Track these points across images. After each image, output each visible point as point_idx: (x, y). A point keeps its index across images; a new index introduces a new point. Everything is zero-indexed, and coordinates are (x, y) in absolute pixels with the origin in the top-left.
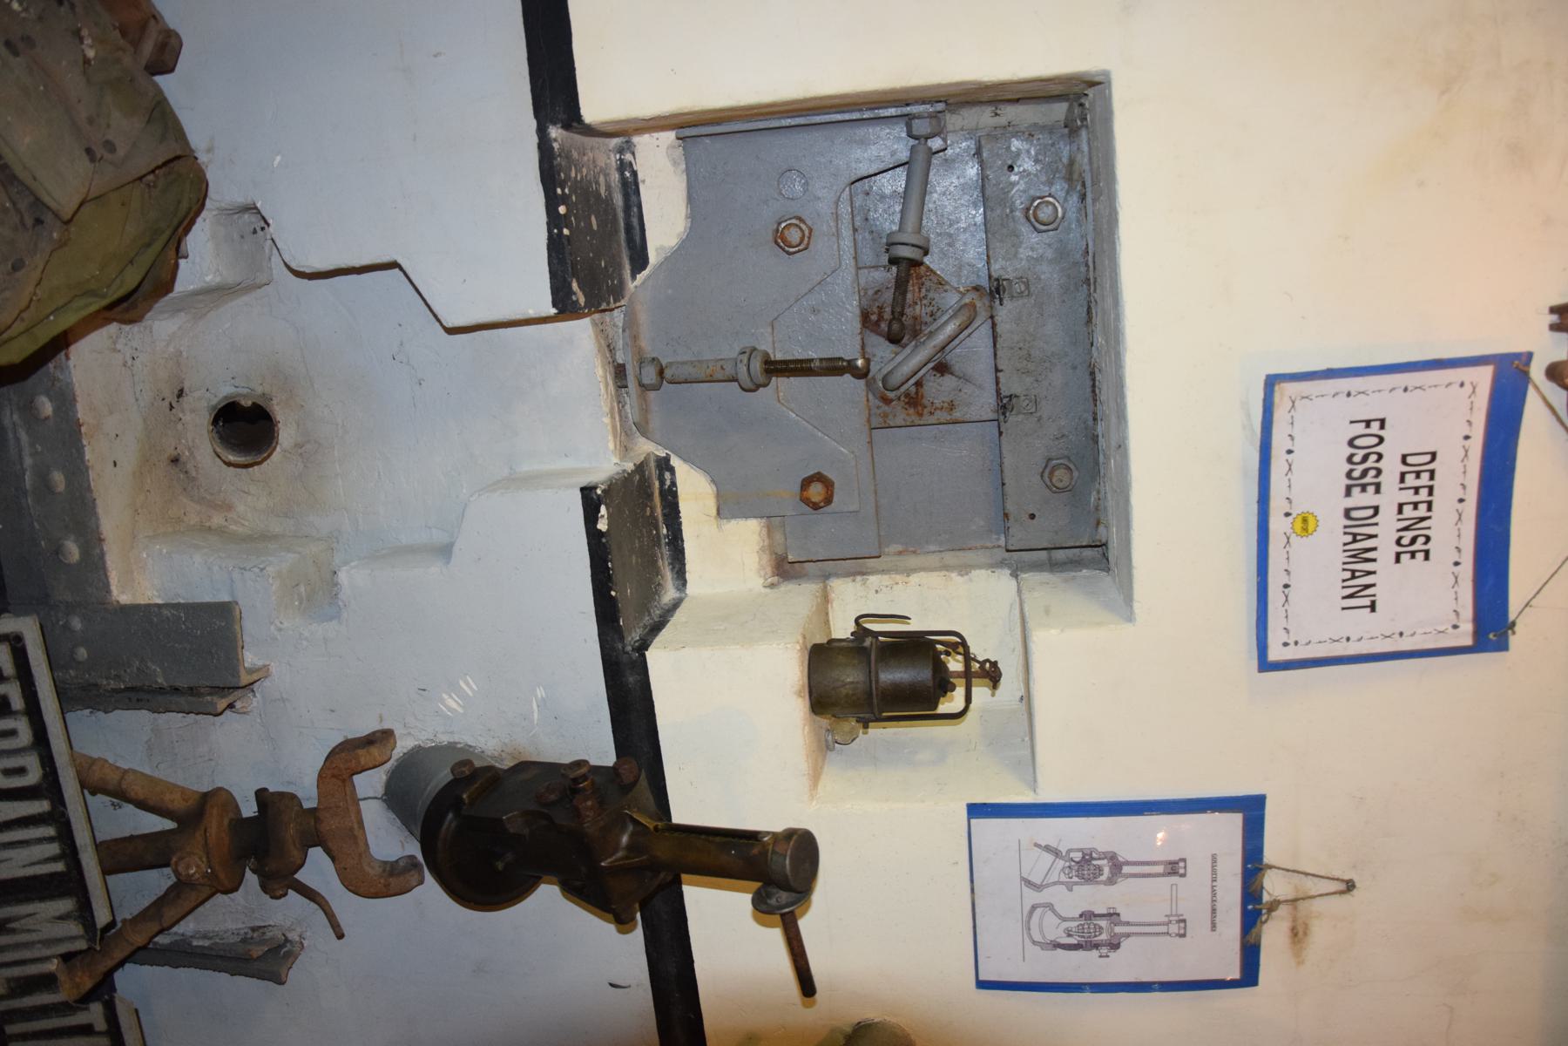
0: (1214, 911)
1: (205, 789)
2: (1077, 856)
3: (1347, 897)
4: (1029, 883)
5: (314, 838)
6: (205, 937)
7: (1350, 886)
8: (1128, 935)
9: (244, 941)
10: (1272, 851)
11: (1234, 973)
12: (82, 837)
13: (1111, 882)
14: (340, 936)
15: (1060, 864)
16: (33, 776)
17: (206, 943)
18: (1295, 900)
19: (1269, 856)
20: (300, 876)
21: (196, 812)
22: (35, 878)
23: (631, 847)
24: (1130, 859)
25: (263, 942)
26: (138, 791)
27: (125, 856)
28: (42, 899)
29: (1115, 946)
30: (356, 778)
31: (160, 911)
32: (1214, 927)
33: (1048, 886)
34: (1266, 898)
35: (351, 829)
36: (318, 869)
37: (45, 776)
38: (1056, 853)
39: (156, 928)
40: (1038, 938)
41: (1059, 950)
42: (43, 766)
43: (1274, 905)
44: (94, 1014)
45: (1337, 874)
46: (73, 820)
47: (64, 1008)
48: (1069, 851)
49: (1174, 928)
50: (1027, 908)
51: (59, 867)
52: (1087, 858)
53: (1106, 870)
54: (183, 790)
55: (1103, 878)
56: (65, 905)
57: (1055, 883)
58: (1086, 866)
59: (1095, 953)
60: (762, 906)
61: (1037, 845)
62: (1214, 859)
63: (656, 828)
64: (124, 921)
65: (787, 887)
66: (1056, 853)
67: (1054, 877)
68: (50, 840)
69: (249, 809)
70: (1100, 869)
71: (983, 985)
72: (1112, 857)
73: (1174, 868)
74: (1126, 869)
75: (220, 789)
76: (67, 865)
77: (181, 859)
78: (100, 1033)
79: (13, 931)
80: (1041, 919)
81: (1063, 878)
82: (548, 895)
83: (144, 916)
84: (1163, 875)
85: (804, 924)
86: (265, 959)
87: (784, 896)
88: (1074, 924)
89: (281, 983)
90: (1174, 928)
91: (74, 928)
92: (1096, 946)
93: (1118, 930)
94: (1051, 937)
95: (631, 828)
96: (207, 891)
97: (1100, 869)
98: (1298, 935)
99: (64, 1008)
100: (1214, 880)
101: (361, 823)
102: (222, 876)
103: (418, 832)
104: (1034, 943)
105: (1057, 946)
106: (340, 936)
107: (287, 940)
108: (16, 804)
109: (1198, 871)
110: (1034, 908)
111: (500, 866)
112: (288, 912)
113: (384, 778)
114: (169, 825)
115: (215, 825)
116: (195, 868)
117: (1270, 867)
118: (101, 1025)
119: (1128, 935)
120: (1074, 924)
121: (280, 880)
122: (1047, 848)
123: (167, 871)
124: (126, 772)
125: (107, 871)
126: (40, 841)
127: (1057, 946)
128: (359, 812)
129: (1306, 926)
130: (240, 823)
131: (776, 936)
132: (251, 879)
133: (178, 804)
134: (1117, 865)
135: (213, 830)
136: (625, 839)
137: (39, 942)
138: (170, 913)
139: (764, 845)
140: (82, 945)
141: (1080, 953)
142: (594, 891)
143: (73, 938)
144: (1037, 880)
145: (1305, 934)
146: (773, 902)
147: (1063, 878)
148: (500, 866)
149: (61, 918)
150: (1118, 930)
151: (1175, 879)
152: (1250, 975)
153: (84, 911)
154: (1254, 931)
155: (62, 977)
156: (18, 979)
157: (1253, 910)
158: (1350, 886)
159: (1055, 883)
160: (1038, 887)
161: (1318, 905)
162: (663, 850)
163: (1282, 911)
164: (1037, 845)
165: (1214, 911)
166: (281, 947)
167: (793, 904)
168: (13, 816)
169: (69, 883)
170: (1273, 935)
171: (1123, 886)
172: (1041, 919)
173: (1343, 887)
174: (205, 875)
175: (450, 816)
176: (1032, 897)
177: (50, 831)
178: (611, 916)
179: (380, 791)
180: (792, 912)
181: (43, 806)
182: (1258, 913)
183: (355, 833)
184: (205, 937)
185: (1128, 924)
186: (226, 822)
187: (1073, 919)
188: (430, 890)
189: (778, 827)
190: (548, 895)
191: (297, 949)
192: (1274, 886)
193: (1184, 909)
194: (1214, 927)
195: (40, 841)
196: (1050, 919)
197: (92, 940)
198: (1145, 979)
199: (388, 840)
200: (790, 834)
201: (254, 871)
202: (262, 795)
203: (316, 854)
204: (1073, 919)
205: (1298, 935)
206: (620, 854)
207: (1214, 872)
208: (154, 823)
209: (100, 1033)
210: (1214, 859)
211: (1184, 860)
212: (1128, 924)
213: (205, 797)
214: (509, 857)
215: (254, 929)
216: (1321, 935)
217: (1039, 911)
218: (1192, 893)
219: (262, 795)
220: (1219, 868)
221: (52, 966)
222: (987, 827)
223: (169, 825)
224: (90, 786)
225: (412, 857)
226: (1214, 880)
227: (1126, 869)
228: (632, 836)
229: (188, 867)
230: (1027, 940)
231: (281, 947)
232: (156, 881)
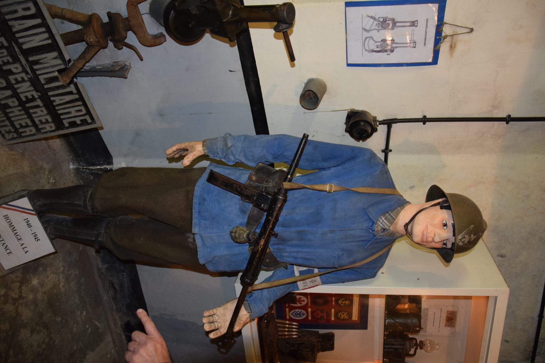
0: (425, 39)
1: (90, 14)
2: (381, 20)
3: (470, 34)
4: (365, 30)
5: (130, 28)
6: (100, 66)
7: (472, 30)
8: (397, 47)
9: (112, 66)
10: (447, 18)
11: (430, 60)
12: (54, 31)
13: (392, 29)
14: (142, 60)
15: (376, 22)
16: (33, 11)
17: (101, 67)
18: (453, 35)
19: (446, 20)
20: (126, 41)
21: (90, 21)
22: (43, 46)
23: (232, 14)
24: (399, 20)
25: (118, 66)
26: (68, 15)
27: (71, 39)
28: (47, 52)
29: (392, 51)
30: (139, 5)
31: (85, 56)
32: (425, 44)
33: (371, 30)
34: (443, 34)
35: (140, 23)
36: (131, 38)
37: (37, 10)
38: (374, 18)
39: (84, 62)
40: (367, 48)
41: (374, 53)
42: (35, 7)
43: (445, 37)
44: (72, 88)
45: (468, 26)
46: (50, 25)
47: (62, 87)
48: (379, 18)
49: (412, 45)
50: (364, 39)
51: (50, 41)
52: (385, 20)
53: (391, 25)
54: (83, 14)
55: (390, 27)
56: (55, 54)
57: (374, 29)
58: (384, 23)
59: (386, 53)
60: (276, 29)
61: (368, 16)
62: (427, 20)
63: (241, 8)
64: (74, 60)
65: (286, 23)
66: (374, 18)
67: (373, 27)
68: (44, 32)
69: (106, 20)
70: (389, 24)
71: (349, 65)
72: (393, 20)
73: (413, 24)
74: (397, 24)
75: (94, 14)
76: (52, 40)
77: (87, 36)
78: (75, 94)
79: (41, 63)
80: (368, 42)
81: (376, 28)
82: (207, 37)
83: (80, 58)
84: (408, 26)
85: (291, 38)
86: (119, 71)
87: (284, 26)
88: (379, 44)
89: (126, 78)
90: (412, 45)
91: (59, 61)
92: (386, 51)
93: (394, 45)
94: (371, 48)
95: (232, 8)
96: (98, 48)
97: (389, 24)
98: (452, 47)
99: (62, 87)
100: (426, 28)
101: (143, 21)
102: (101, 42)
103: (162, 21)
104: (366, 50)
105: (374, 51)
106: (142, 60)
107: (125, 65)
108: (30, 21)
109: (421, 24)
110: (366, 38)
111: (190, 26)
112: (124, 55)
113: (149, 6)
114: (80, 27)
115: (96, 25)
116: (92, 39)
117: (446, 23)
118: (75, 91)
119: (397, 47)
120: (379, 44)
121: (120, 43)
122: (372, 17)
123: (84, 43)
124: (63, 9)
125: (66, 44)
126: (41, 33)
127: (374, 51)
128: (142, 18)
129: (455, 44)
130: (103, 25)
131: (281, 43)
132: (111, 44)
133: (82, 19)
134: (394, 23)
135: (95, 27)
136: (231, 12)
137: (50, 66)
138: (88, 56)
139: (277, 8)
140: (63, 67)
141: (381, 54)
142: (221, 32)
143: (60, 65)
144: (367, 28)
145: (455, 47)
146: (281, 28)
147: (376, 28)
148: (190, 26)
149: (55, 58)
150: (394, 45)
151: (413, 28)
152: (435, 61)
153: (61, 55)
154: (438, 46)
155: (60, 78)
156: (47, 78)
157: (439, 38)
158: (472, 30)
159: (374, 29)
160: (367, 31)
161: (460, 37)
162: (244, 15)
163: (448, 39)
164: (368, 16)
165: (425, 39)
166: (124, 67)
167: (287, 28)
168: (31, 25)
169: (53, 47)
170: (444, 47)
171: (397, 30)
172: (368, 42)
173: (469, 30)
174: (96, 42)
175: (172, 12)
176: (366, 34)
177: (44, 29)
178: (227, 40)
179: (148, 11)
180: (286, 31)
181: (38, 21)
182: (440, 39)
183: (142, 25)
184: (100, 66)
185: (397, 43)
186: (99, 24)
187: (379, 42)
188: (170, 41)
189: (281, 3)
190: (207, 37)
191: (129, 67)
192: (446, 30)
193: (416, 38)
194: (425, 44)
195: (41, 33)
196: (371, 42)
197: (65, 65)
198: (401, 62)
199: (153, 27)
200: (285, 4)
201: (111, 41)
202: (109, 14)
203: (130, 34)
204: (379, 42)
205: (452, 47)
206: (230, 17)
207: (427, 25)
208: (75, 27)
209: (75, 94)
210: (427, 20)
211: (417, 21)
212: (397, 43)
213: (91, 16)
214: (193, 22)
215: (115, 62)
216: (460, 48)
217: (368, 39)
218: (420, 30)
219: (109, 14)
220: (429, 24)
221: (56, 74)
222: (350, 9)
223: (80, 27)
224: (54, 16)
225: (162, 33)
226: (426, 28)
227: (397, 24)
228: (233, 11)
229: (90, 39)
230: (364, 50)
231: (124, 67)
232: (81, 47)
